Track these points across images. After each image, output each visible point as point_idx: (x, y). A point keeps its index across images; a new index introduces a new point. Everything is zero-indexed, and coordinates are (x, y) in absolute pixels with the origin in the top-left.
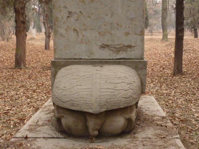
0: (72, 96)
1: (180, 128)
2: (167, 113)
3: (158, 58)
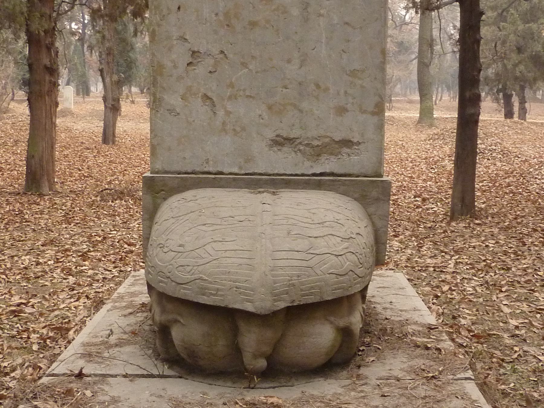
0: (200, 268)
1: (471, 354)
2: (439, 316)
3: (409, 173)
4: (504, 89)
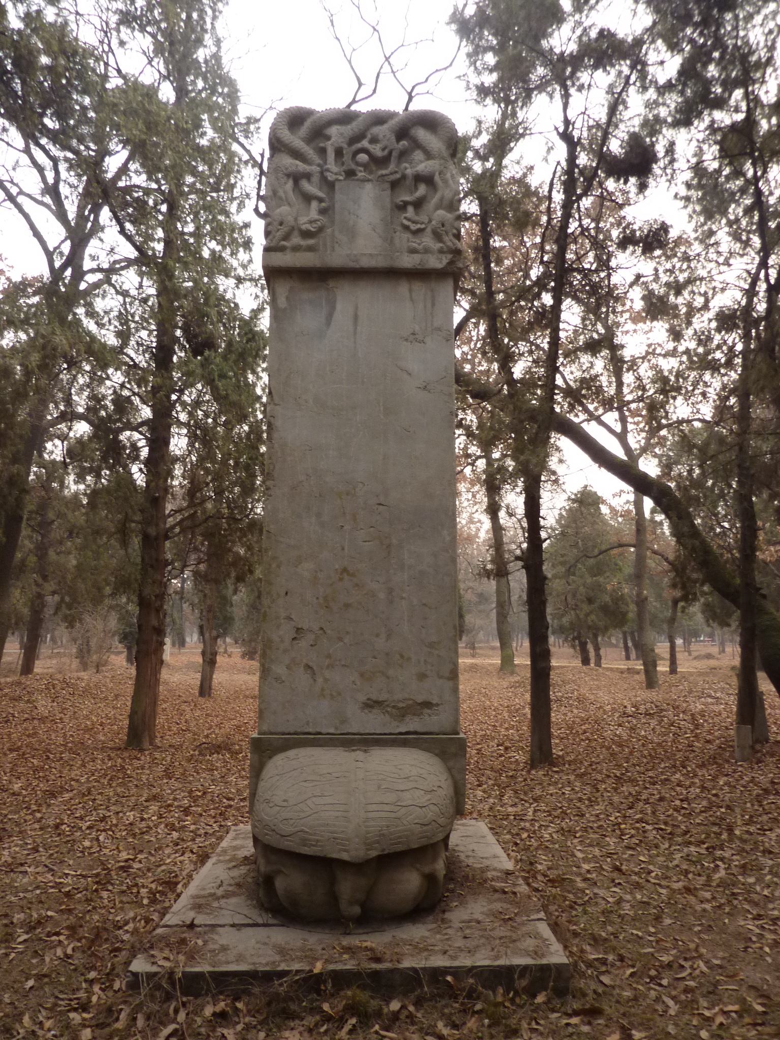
4: (578, 637)
